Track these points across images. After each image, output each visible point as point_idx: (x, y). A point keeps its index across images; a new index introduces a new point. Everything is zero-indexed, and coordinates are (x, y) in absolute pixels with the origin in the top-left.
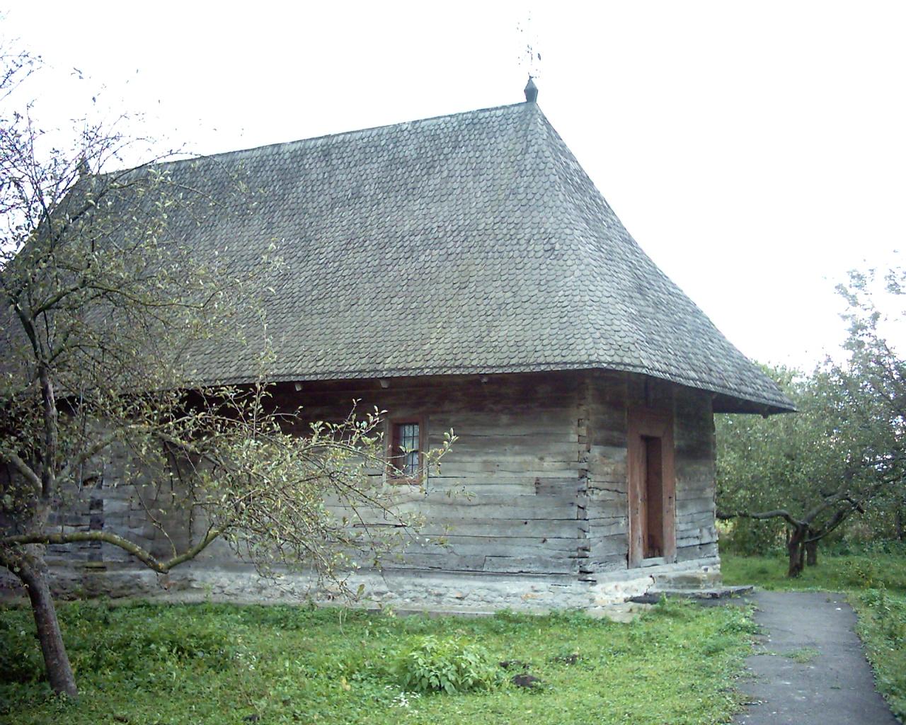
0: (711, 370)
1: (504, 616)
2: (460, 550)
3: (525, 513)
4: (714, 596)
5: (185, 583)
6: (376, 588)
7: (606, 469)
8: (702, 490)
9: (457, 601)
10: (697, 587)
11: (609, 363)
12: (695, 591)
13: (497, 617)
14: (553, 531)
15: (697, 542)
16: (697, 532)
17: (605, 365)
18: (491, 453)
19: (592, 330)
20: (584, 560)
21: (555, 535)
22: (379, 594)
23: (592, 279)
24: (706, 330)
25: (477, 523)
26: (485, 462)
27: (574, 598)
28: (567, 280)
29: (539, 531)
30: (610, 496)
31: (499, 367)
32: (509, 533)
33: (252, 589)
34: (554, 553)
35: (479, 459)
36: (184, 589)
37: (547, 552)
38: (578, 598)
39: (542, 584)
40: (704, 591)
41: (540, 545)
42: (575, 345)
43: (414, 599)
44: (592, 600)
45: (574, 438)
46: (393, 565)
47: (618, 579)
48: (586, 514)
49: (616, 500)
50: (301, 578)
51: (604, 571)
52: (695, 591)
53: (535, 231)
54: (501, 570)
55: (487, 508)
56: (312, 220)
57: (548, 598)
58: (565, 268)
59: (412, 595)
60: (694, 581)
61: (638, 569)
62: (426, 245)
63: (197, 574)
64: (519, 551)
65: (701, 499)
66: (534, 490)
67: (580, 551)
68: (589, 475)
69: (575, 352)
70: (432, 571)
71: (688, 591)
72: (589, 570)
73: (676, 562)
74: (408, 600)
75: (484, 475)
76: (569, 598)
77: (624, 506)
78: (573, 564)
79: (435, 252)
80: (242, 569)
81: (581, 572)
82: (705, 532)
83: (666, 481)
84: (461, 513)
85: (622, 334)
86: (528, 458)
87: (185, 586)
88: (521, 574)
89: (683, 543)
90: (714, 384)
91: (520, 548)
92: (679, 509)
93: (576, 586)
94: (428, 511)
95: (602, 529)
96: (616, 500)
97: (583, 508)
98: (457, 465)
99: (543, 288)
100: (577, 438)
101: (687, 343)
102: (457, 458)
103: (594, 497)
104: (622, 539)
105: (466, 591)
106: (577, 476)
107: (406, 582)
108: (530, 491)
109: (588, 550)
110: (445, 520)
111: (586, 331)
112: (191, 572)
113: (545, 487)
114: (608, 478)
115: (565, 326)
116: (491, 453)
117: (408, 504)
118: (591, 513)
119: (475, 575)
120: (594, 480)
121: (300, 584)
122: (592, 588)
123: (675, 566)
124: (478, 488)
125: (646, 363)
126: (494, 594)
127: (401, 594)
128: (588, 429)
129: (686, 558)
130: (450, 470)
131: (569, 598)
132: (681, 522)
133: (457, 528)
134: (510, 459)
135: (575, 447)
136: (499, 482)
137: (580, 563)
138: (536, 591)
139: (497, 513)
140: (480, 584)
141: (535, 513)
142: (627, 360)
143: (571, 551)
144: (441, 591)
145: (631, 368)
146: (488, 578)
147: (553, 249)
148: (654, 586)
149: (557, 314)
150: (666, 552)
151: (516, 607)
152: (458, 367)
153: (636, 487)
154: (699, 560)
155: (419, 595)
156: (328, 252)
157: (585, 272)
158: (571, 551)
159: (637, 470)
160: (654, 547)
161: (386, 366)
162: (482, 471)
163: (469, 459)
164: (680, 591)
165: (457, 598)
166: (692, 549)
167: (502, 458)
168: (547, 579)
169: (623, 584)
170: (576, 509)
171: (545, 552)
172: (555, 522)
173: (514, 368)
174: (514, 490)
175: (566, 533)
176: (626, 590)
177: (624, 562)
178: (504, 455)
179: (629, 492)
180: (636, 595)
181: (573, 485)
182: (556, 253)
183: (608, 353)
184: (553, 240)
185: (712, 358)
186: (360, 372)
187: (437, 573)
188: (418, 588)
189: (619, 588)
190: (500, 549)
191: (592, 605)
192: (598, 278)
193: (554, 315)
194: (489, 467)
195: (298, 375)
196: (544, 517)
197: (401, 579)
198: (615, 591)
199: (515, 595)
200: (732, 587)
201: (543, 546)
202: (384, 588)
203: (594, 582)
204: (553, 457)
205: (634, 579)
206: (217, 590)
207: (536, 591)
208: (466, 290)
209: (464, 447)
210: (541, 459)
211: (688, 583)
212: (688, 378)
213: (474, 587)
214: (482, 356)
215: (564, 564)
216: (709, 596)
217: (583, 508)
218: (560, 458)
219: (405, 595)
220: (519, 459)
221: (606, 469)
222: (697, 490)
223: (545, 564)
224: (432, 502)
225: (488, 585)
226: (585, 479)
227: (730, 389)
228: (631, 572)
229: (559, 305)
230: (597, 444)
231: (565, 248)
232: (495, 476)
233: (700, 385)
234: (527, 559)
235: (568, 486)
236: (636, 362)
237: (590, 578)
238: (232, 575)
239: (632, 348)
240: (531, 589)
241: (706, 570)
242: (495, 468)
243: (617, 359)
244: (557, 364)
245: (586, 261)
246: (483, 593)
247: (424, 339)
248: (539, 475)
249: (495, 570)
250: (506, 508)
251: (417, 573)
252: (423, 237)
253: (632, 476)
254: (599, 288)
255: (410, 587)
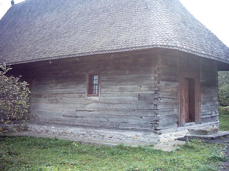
0: (213, 52)
1: (121, 147)
2: (111, 120)
3: (134, 107)
4: (212, 138)
5: (26, 128)
6: (82, 133)
7: (167, 90)
8: (213, 97)
9: (109, 138)
10: (206, 134)
11: (161, 45)
12: (205, 136)
13: (118, 147)
14: (145, 114)
15: (210, 116)
16: (210, 112)
17: (159, 46)
18: (122, 85)
19: (156, 34)
20: (156, 125)
21: (145, 115)
22: (83, 134)
23: (161, 16)
24: (215, 39)
25: (117, 110)
26: (120, 88)
27: (152, 139)
28: (151, 17)
29: (139, 114)
30: (169, 101)
31: (117, 50)
32: (128, 114)
33: (45, 131)
34: (144, 122)
35: (118, 87)
36: (26, 130)
37: (142, 122)
38: (153, 140)
39: (140, 134)
40: (208, 136)
41: (140, 119)
42: (148, 39)
43: (95, 137)
44: (159, 141)
45: (153, 78)
46: (88, 125)
47: (172, 132)
48: (157, 108)
49: (173, 102)
50: (59, 128)
51: (166, 129)
52: (205, 136)
53: (142, 3)
54: (125, 128)
55: (120, 105)
56: (71, 9)
57: (142, 139)
58: (151, 13)
59: (94, 135)
60: (205, 132)
61: (182, 127)
62: (103, 11)
63: (30, 126)
64: (132, 121)
65: (211, 101)
66: (138, 98)
67: (155, 121)
68: (159, 92)
69: (148, 42)
70: (101, 127)
71: (202, 136)
72: (158, 129)
73: (200, 124)
74: (93, 137)
75: (120, 93)
76: (150, 139)
77: (177, 104)
78: (152, 126)
79: (106, 14)
80: (42, 125)
81: (155, 130)
82: (213, 112)
83: (197, 94)
84: (111, 107)
85: (170, 35)
86: (136, 86)
87: (26, 129)
88: (132, 130)
89: (204, 117)
90: (214, 57)
91: (132, 120)
92: (202, 105)
93: (152, 135)
94: (101, 106)
95: (165, 113)
96: (173, 102)
97: (156, 105)
98: (110, 89)
99: (141, 21)
100: (154, 78)
101: (203, 42)
102: (111, 87)
103: (162, 101)
104: (175, 116)
105: (112, 135)
106: (154, 93)
107: (92, 131)
108: (136, 99)
109: (159, 121)
110: (106, 109)
111: (154, 34)
112: (28, 125)
113: (142, 97)
114: (169, 94)
115: (146, 33)
116: (122, 85)
117: (92, 104)
118: (159, 107)
119: (116, 129)
120: (161, 94)
121: (59, 130)
122: (159, 136)
123: (200, 125)
124: (117, 97)
125: (178, 45)
126: (122, 136)
127: (90, 135)
128: (159, 74)
129: (205, 122)
130: (108, 91)
131: (150, 139)
132: (203, 109)
133: (110, 112)
134: (129, 87)
135: (153, 82)
136: (124, 95)
137: (154, 126)
138: (137, 136)
139: (124, 107)
140: (118, 133)
141: (138, 107)
142: (169, 44)
143: (151, 121)
144: (104, 134)
145: (171, 48)
146: (120, 130)
147: (148, 8)
148: (189, 133)
149: (144, 29)
150: (196, 120)
151: (127, 143)
152: (102, 51)
153: (182, 97)
154: (210, 123)
155: (96, 135)
156: (72, 18)
157: (158, 15)
158: (151, 121)
159: (54, 91)
160: (191, 118)
161: (78, 52)
162: (119, 92)
163: (115, 87)
164: (199, 136)
165: (109, 137)
166: (208, 119)
167: (126, 87)
168: (142, 132)
169: (174, 133)
170: (153, 105)
171: (142, 122)
172: (145, 110)
173: (123, 50)
174: (131, 98)
175: (150, 114)
176: (176, 136)
177: (176, 125)
178: (127, 85)
179: (179, 99)
180: (180, 137)
181: (152, 96)
182: (148, 9)
183: (161, 42)
184: (148, 5)
185: (214, 48)
186: (69, 55)
187: (103, 128)
188: (96, 133)
189: (172, 135)
190: (125, 120)
191: (159, 142)
192: (164, 17)
193: (142, 30)
194: (122, 90)
195: (50, 58)
196: (141, 108)
197: (90, 129)
198: (169, 137)
199: (130, 137)
200: (224, 132)
201: (141, 119)
202: (85, 133)
203: (160, 134)
204: (145, 86)
205: (180, 131)
206: (35, 131)
207: (137, 136)
208: (113, 25)
209: (113, 83)
210: (140, 86)
211: (202, 132)
212: (201, 54)
213: (115, 133)
214: (112, 46)
215: (149, 126)
216: (210, 138)
217: (156, 105)
218: (147, 86)
219: (92, 135)
220: (132, 87)
221: (167, 90)
222: (210, 97)
223: (141, 126)
224: (101, 103)
225: (120, 133)
226: (157, 94)
227: (222, 59)
228: (179, 128)
229: (146, 26)
230: (163, 80)
231: (152, 7)
232: (124, 93)
233: (206, 56)
234: (134, 124)
235: (150, 96)
236: (174, 45)
237: (158, 132)
238: (39, 126)
239: (173, 40)
240: (135, 135)
241: (213, 126)
242: (124, 90)
243: (165, 44)
244: (139, 47)
245: (159, 11)
246: (118, 136)
247: (95, 42)
248: (140, 92)
249: (123, 128)
250: (127, 105)
251: (96, 128)
252: (103, 9)
253: (181, 93)
254: (163, 20)
255: (94, 133)
